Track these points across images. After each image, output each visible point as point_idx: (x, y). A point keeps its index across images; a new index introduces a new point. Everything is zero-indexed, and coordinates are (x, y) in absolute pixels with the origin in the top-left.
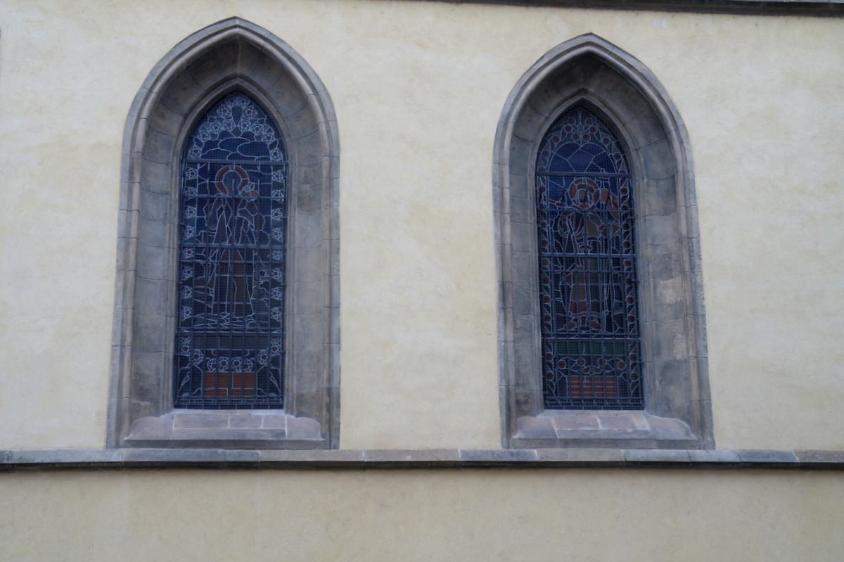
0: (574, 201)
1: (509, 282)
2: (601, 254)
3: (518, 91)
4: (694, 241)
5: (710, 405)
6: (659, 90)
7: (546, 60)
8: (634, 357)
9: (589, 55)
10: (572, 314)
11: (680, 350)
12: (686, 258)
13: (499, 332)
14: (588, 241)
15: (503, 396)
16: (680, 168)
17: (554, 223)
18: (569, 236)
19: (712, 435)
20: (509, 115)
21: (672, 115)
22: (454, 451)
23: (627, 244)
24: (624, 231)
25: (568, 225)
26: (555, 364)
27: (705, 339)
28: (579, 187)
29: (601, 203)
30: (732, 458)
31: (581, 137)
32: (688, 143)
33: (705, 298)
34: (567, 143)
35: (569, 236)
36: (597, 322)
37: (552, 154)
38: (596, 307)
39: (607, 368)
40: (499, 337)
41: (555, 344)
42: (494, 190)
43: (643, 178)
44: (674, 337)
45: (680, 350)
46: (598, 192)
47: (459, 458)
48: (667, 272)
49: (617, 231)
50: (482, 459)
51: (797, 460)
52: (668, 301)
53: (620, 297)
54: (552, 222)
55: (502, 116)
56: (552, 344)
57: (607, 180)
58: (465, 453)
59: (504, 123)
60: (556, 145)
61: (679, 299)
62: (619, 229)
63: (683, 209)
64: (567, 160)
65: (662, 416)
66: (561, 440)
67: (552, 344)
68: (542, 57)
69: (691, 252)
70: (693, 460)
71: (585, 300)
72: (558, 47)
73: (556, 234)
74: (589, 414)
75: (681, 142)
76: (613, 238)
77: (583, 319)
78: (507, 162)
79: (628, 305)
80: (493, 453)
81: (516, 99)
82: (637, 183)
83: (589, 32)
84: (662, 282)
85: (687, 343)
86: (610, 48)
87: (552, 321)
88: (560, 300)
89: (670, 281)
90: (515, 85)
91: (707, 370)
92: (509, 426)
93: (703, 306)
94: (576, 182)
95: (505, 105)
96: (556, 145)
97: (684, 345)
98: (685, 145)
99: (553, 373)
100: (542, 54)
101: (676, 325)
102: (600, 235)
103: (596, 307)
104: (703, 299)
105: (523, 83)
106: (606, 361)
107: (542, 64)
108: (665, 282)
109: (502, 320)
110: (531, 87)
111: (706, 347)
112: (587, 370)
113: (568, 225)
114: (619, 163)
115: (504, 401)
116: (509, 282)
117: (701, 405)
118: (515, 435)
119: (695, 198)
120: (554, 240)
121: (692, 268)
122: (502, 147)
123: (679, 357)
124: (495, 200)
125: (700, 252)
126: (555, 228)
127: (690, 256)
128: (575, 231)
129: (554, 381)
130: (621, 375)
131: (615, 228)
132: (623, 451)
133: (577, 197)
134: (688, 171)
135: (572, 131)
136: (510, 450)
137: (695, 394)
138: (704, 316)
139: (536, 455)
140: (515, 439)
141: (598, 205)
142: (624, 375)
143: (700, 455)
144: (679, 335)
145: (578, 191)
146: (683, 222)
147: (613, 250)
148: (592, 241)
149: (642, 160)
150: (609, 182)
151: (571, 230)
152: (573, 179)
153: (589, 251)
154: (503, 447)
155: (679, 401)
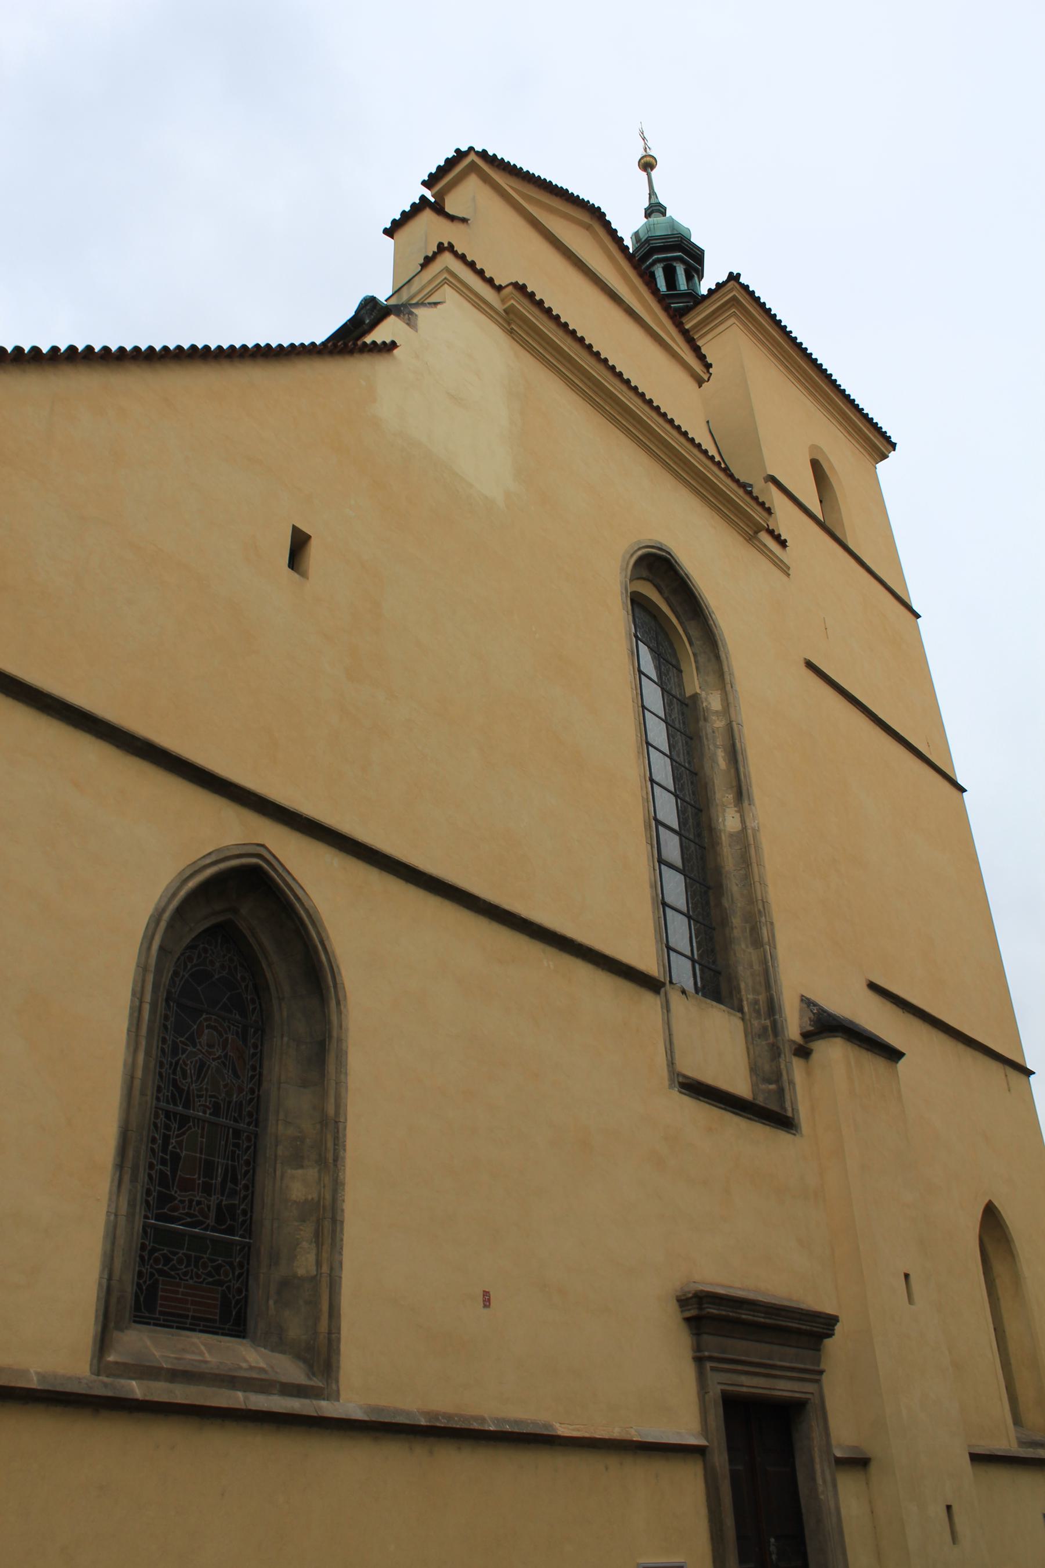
0: (200, 1042)
1: (132, 1131)
2: (228, 1121)
3: (178, 884)
4: (341, 1126)
5: (339, 1340)
6: (323, 935)
7: (213, 858)
8: (241, 1265)
9: (256, 870)
10: (178, 1193)
11: (305, 1264)
12: (330, 1144)
13: (110, 1199)
14: (208, 1099)
15: (103, 1294)
16: (335, 1034)
17: (174, 1064)
18: (189, 1088)
19: (337, 1381)
20: (164, 910)
21: (333, 969)
22: (24, 1373)
23: (250, 1115)
24: (249, 1097)
25: (189, 1071)
26: (149, 1259)
27: (341, 1254)
28: (208, 1027)
29: (229, 1053)
30: (359, 1415)
31: (218, 964)
32: (345, 1006)
33: (345, 1200)
34: (202, 968)
35: (189, 1088)
36: (206, 1209)
37: (183, 976)
38: (207, 1189)
39: (210, 1274)
40: (109, 1206)
41: (153, 1230)
42: (132, 1001)
43: (282, 1036)
44: (298, 1244)
45: (305, 1264)
46: (227, 1039)
47: (34, 1384)
48: (297, 1160)
49: (241, 1095)
50: (69, 1388)
51: (423, 1422)
52: (294, 1197)
53: (235, 1181)
54: (171, 1065)
55: (156, 909)
56: (149, 1231)
57: (238, 1027)
58: (42, 1377)
59: (156, 919)
60: (189, 967)
61: (310, 1197)
62: (245, 1093)
63: (333, 1084)
64: (199, 989)
65: (272, 1351)
66: (168, 1370)
67: (149, 1231)
68: (210, 854)
69: (336, 1138)
70: (321, 1414)
71: (196, 1176)
72: (227, 848)
73: (174, 1080)
74: (188, 1337)
75: (338, 1003)
76: (236, 1102)
77: (191, 1201)
78: (152, 968)
79: (243, 1193)
80: (79, 1380)
81: (174, 895)
82: (275, 1039)
83: (262, 843)
84: (289, 1171)
85: (318, 1255)
86: (280, 870)
87: (154, 1198)
88: (167, 1170)
89: (300, 1171)
90: (176, 876)
91: (339, 1293)
92: (103, 1343)
93: (343, 1210)
94: (206, 1020)
95: (161, 897)
96: (189, 967)
97: (312, 1257)
98: (342, 1007)
99: (145, 1271)
100: (211, 850)
101: (302, 1230)
102: (223, 1095)
103: (207, 1189)
104: (344, 1201)
105: (185, 876)
106: (210, 1264)
107: (208, 861)
108: (294, 1172)
109: (116, 1183)
110: (191, 884)
111: (341, 1263)
112: (185, 1274)
113: (189, 1071)
114: (254, 1009)
115: (103, 1302)
116: (132, 1131)
117: (330, 1341)
118: (109, 1356)
119: (346, 1074)
120: (171, 1088)
121: (336, 1160)
122: (149, 948)
123: (301, 1272)
124: (131, 1015)
125: (345, 1141)
126: (174, 1073)
127: (335, 1145)
128: (196, 1082)
129: (145, 1282)
130: (224, 1288)
131: (240, 1090)
132: (240, 1394)
133: (204, 1039)
134: (342, 1040)
135: (208, 955)
136: (100, 1378)
137: (323, 1325)
138: (342, 1222)
139: (136, 1389)
140: (109, 1362)
141: (226, 1056)
142: (228, 1288)
143: (328, 1408)
144: (305, 1244)
145: (206, 1031)
146: (332, 1100)
147: (234, 1117)
148: (213, 1100)
149: (285, 1014)
150: (240, 1030)
151: (192, 1081)
152: (202, 1016)
153: (208, 1112)
154: (92, 1373)
155: (295, 1331)
